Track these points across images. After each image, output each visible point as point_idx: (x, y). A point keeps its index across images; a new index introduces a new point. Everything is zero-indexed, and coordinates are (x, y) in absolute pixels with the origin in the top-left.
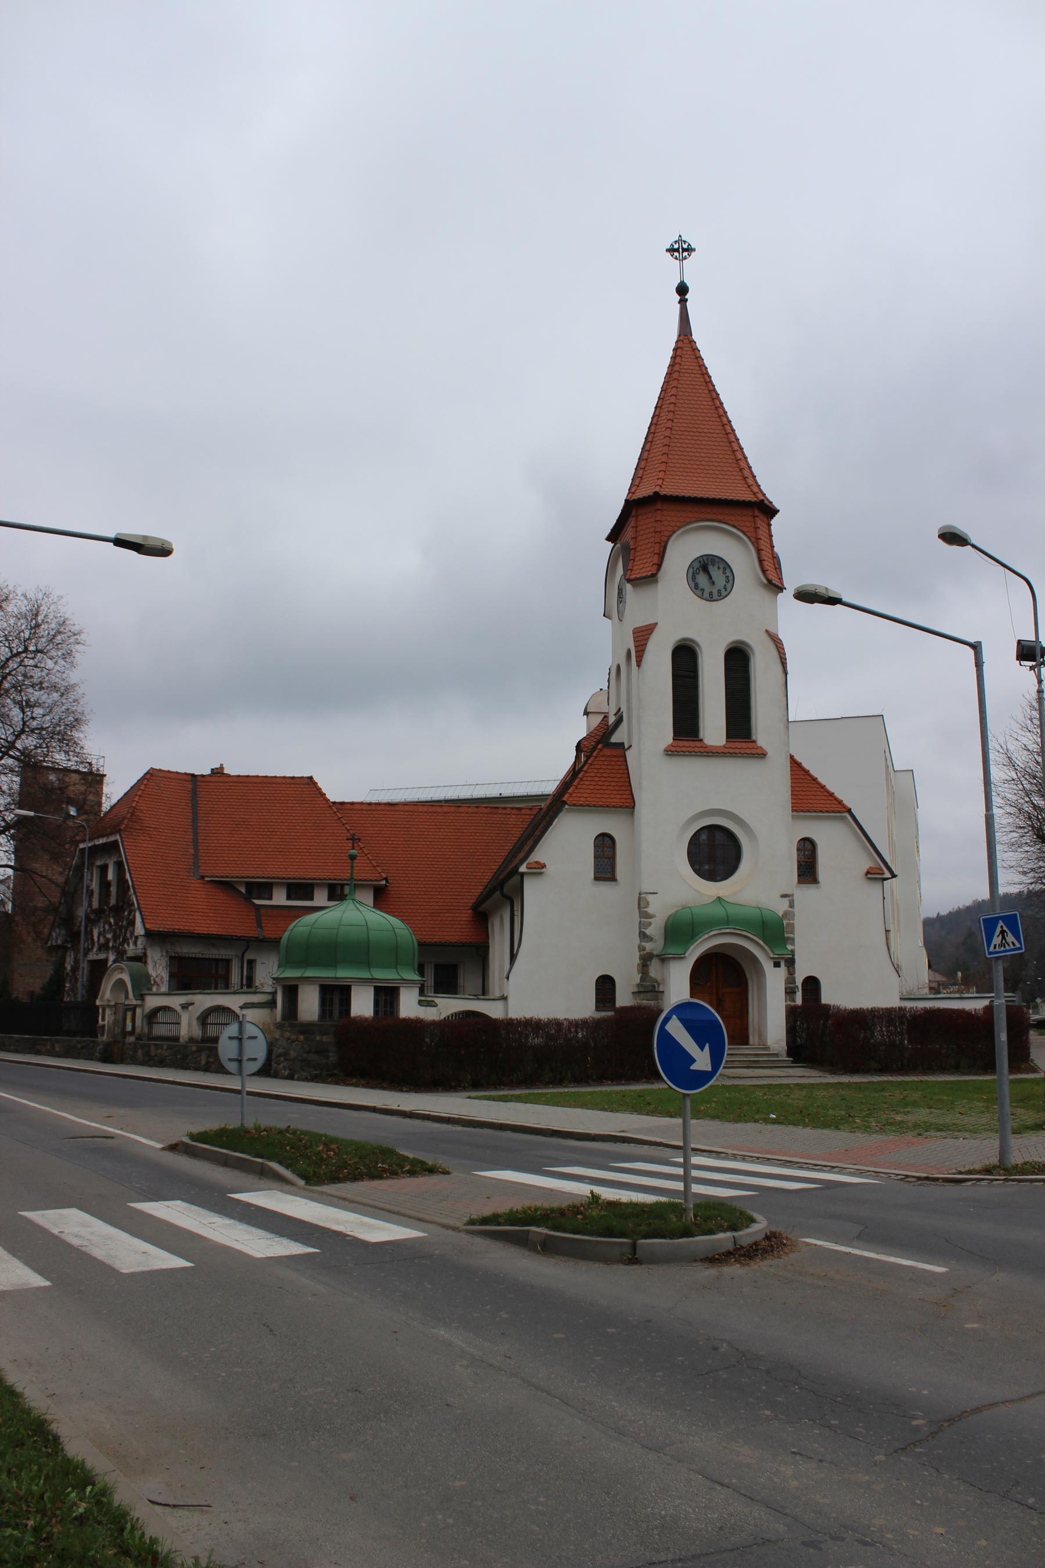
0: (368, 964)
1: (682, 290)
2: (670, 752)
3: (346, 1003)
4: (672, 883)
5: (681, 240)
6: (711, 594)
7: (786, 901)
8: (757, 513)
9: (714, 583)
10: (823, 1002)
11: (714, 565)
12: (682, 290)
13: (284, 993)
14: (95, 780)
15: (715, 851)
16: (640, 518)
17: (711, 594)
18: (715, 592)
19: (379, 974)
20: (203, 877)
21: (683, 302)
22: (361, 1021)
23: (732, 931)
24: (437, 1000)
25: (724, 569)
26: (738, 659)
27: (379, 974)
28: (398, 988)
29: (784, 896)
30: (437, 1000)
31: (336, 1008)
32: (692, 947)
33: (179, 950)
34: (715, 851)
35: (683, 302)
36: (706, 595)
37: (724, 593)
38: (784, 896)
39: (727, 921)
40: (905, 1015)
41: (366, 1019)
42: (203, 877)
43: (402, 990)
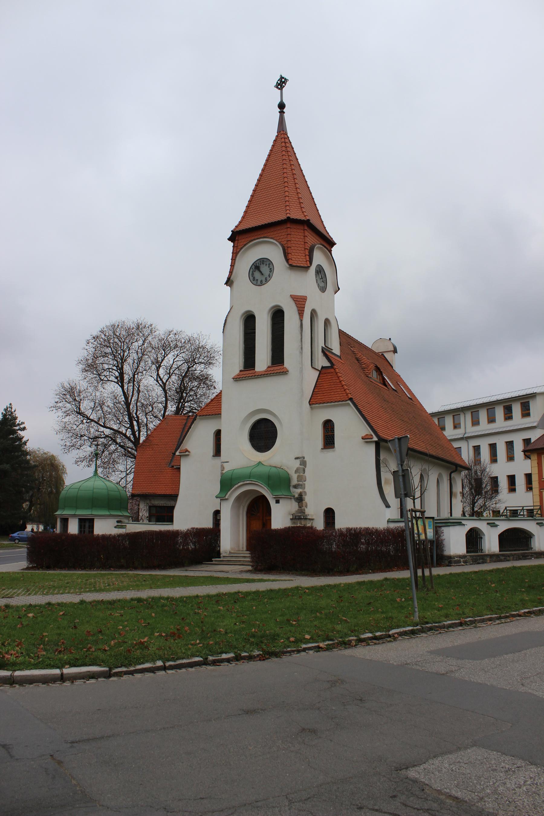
0: (77, 508)
1: (282, 106)
2: (237, 379)
3: (92, 527)
4: (240, 453)
5: (282, 78)
6: (261, 281)
7: (298, 461)
8: (306, 228)
9: (262, 274)
10: (211, 527)
11: (263, 264)
12: (282, 106)
13: (61, 522)
14: (16, 418)
15: (263, 434)
16: (239, 242)
17: (261, 281)
18: (264, 279)
19: (79, 512)
20: (173, 466)
21: (282, 113)
22: (73, 536)
23: (250, 482)
24: (497, 523)
25: (269, 264)
26: (278, 316)
27: (79, 512)
28: (94, 519)
29: (296, 458)
30: (497, 523)
31: (87, 530)
32: (229, 493)
33: (153, 503)
34: (263, 434)
35: (282, 113)
36: (259, 282)
37: (268, 279)
38: (296, 458)
39: (250, 476)
40: (394, 532)
41: (75, 535)
42: (173, 466)
43: (95, 520)
